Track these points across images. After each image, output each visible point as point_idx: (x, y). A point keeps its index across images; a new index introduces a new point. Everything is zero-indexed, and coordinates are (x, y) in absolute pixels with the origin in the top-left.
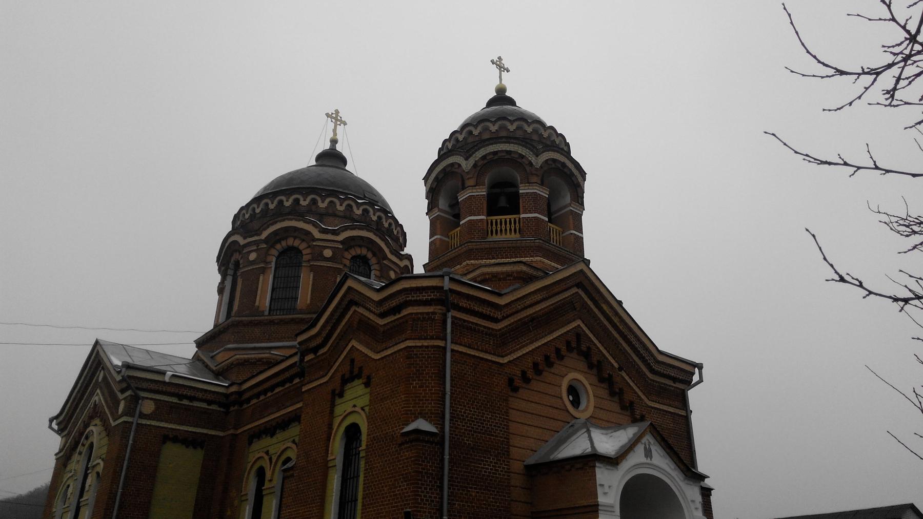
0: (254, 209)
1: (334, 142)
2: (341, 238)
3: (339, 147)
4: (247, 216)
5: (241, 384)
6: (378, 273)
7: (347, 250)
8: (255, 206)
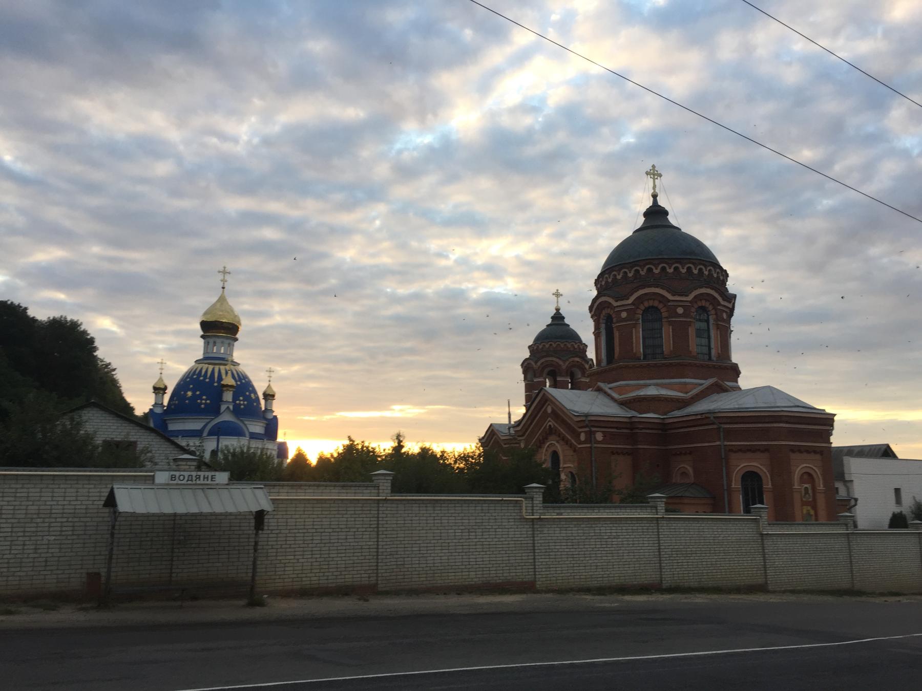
1: (655, 196)
3: (662, 202)
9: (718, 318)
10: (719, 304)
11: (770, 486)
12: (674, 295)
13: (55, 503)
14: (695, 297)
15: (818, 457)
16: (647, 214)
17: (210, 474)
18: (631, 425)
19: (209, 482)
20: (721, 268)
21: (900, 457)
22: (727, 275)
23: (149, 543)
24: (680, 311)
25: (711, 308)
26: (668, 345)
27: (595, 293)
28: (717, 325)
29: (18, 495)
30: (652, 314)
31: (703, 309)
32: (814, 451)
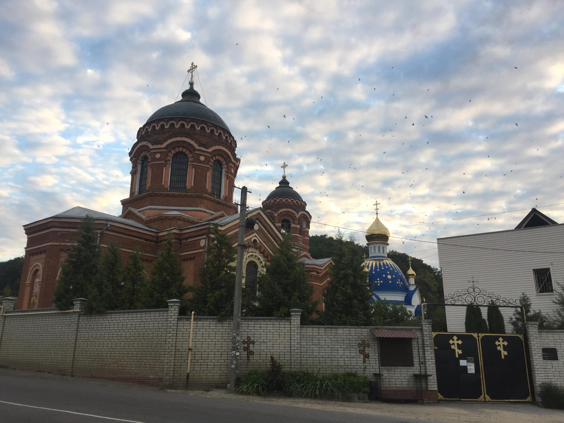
0: (147, 129)
1: (191, 84)
2: (210, 150)
3: (196, 88)
4: (143, 133)
5: (181, 230)
6: (226, 169)
7: (170, 152)
8: (147, 127)
12: (200, 146)
13: (204, 340)
14: (214, 151)
16: (184, 94)
21: (559, 223)
24: (202, 158)
25: (224, 163)
26: (190, 182)
27: (136, 140)
28: (227, 176)
30: (180, 159)
31: (218, 162)
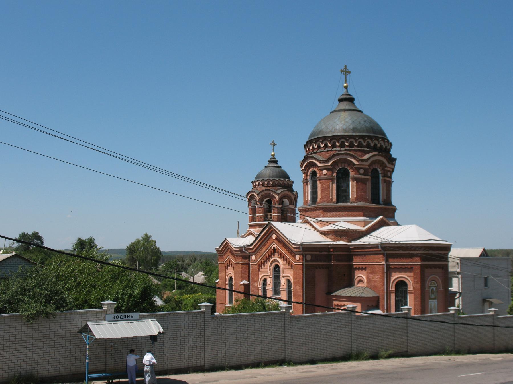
9: (385, 176)
10: (386, 166)
11: (412, 289)
15: (440, 270)
17: (130, 314)
18: (326, 248)
19: (130, 318)
20: (388, 141)
22: (391, 145)
23: (28, 337)
29: (34, 327)
32: (439, 267)
